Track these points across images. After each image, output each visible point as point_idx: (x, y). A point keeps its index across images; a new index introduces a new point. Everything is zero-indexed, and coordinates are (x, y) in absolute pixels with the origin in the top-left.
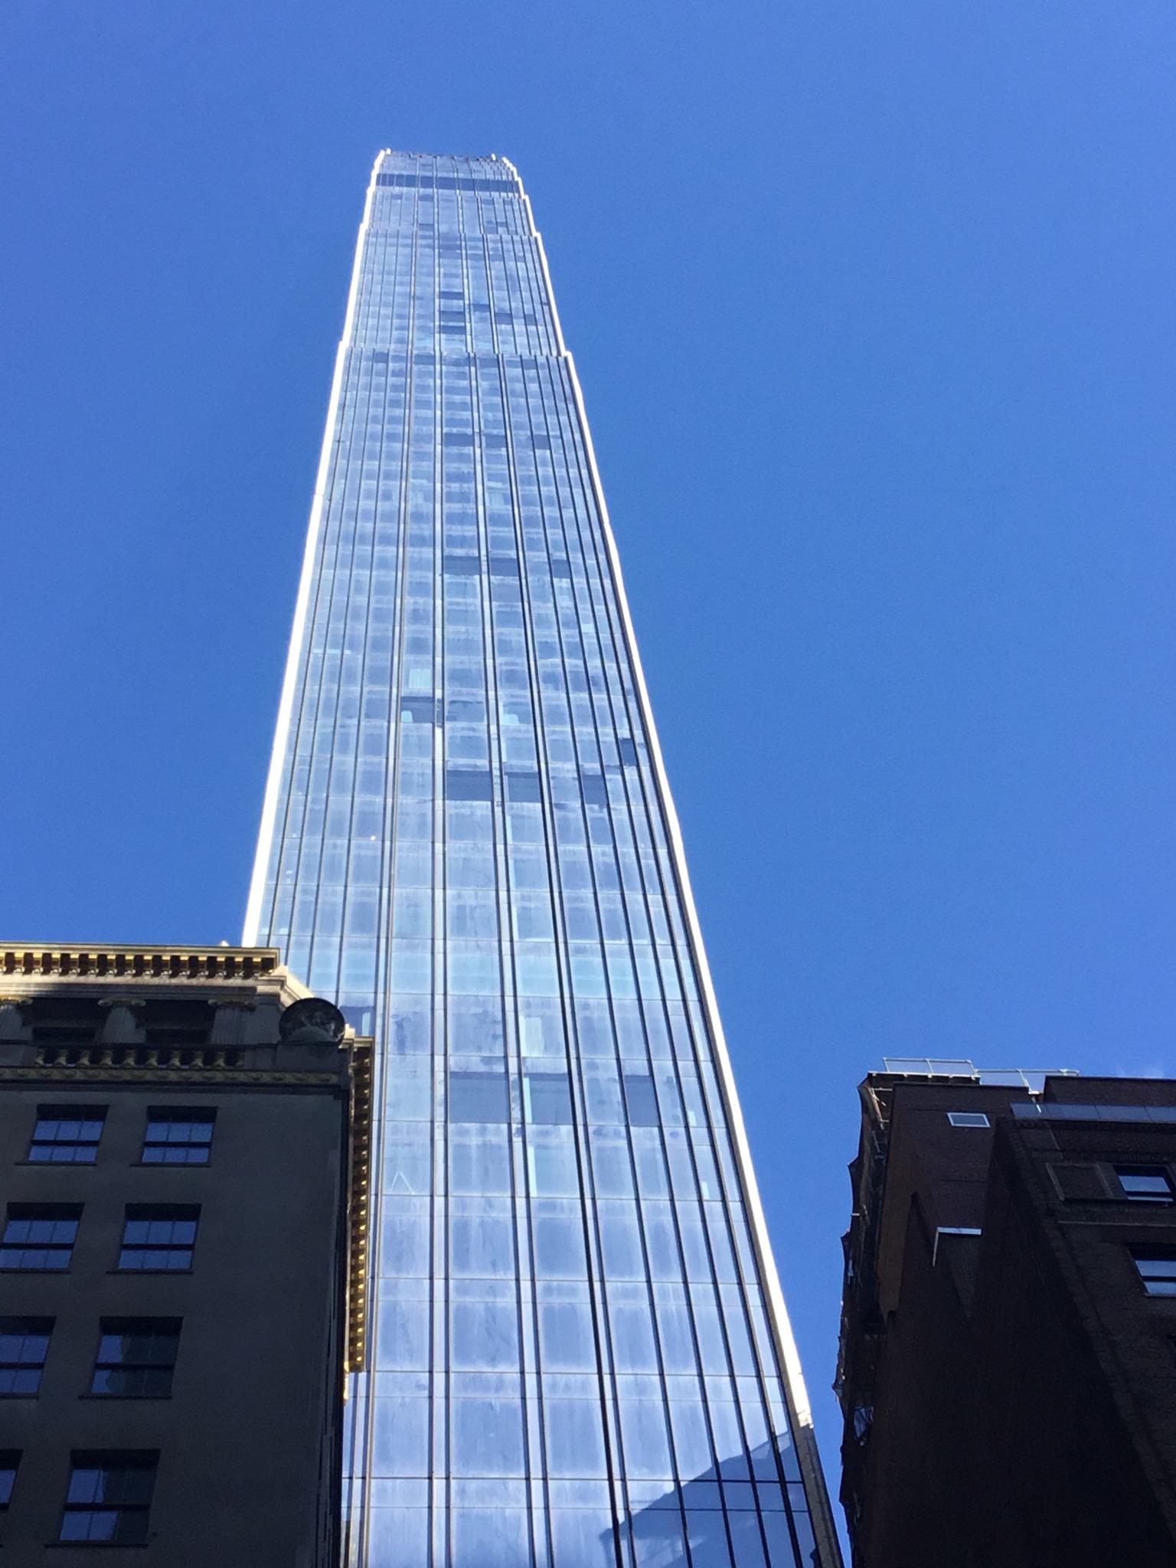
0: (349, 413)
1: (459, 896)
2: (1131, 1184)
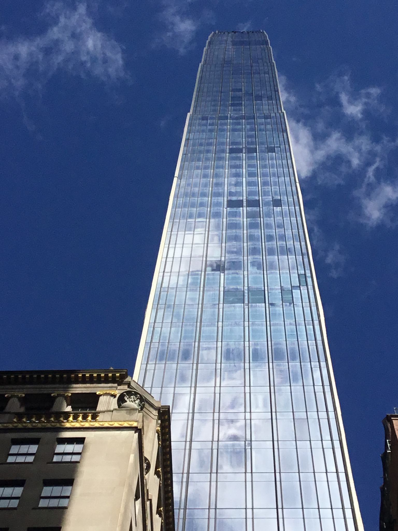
0: (191, 142)
1: (228, 344)
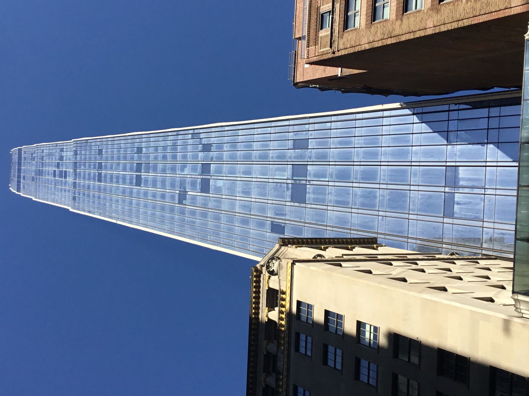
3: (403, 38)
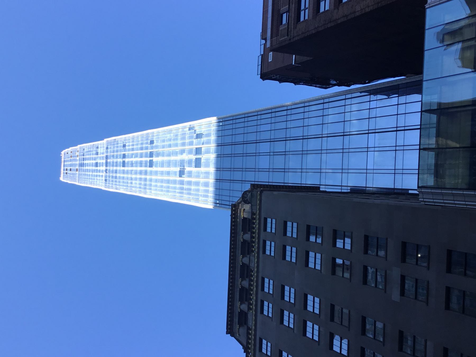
2: (284, 22)
3: (339, 22)
